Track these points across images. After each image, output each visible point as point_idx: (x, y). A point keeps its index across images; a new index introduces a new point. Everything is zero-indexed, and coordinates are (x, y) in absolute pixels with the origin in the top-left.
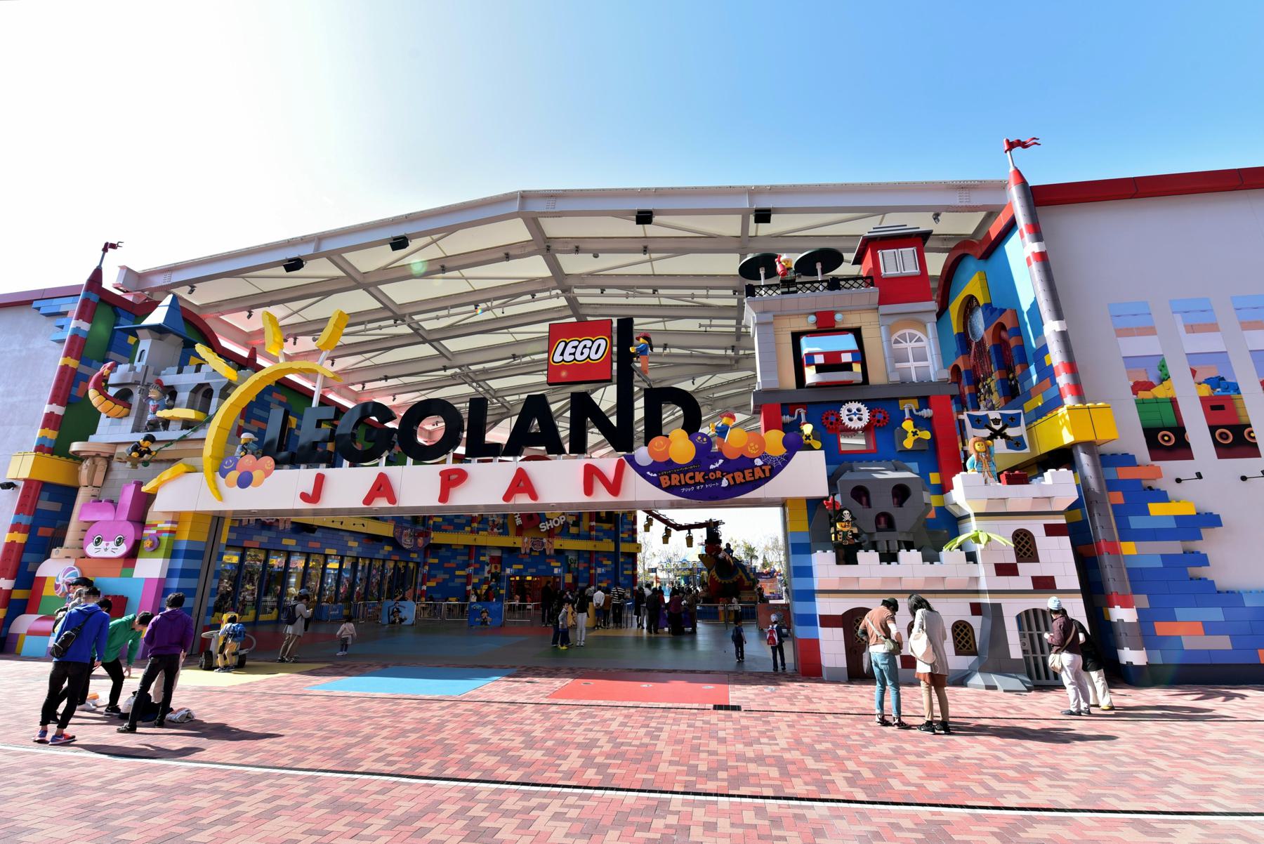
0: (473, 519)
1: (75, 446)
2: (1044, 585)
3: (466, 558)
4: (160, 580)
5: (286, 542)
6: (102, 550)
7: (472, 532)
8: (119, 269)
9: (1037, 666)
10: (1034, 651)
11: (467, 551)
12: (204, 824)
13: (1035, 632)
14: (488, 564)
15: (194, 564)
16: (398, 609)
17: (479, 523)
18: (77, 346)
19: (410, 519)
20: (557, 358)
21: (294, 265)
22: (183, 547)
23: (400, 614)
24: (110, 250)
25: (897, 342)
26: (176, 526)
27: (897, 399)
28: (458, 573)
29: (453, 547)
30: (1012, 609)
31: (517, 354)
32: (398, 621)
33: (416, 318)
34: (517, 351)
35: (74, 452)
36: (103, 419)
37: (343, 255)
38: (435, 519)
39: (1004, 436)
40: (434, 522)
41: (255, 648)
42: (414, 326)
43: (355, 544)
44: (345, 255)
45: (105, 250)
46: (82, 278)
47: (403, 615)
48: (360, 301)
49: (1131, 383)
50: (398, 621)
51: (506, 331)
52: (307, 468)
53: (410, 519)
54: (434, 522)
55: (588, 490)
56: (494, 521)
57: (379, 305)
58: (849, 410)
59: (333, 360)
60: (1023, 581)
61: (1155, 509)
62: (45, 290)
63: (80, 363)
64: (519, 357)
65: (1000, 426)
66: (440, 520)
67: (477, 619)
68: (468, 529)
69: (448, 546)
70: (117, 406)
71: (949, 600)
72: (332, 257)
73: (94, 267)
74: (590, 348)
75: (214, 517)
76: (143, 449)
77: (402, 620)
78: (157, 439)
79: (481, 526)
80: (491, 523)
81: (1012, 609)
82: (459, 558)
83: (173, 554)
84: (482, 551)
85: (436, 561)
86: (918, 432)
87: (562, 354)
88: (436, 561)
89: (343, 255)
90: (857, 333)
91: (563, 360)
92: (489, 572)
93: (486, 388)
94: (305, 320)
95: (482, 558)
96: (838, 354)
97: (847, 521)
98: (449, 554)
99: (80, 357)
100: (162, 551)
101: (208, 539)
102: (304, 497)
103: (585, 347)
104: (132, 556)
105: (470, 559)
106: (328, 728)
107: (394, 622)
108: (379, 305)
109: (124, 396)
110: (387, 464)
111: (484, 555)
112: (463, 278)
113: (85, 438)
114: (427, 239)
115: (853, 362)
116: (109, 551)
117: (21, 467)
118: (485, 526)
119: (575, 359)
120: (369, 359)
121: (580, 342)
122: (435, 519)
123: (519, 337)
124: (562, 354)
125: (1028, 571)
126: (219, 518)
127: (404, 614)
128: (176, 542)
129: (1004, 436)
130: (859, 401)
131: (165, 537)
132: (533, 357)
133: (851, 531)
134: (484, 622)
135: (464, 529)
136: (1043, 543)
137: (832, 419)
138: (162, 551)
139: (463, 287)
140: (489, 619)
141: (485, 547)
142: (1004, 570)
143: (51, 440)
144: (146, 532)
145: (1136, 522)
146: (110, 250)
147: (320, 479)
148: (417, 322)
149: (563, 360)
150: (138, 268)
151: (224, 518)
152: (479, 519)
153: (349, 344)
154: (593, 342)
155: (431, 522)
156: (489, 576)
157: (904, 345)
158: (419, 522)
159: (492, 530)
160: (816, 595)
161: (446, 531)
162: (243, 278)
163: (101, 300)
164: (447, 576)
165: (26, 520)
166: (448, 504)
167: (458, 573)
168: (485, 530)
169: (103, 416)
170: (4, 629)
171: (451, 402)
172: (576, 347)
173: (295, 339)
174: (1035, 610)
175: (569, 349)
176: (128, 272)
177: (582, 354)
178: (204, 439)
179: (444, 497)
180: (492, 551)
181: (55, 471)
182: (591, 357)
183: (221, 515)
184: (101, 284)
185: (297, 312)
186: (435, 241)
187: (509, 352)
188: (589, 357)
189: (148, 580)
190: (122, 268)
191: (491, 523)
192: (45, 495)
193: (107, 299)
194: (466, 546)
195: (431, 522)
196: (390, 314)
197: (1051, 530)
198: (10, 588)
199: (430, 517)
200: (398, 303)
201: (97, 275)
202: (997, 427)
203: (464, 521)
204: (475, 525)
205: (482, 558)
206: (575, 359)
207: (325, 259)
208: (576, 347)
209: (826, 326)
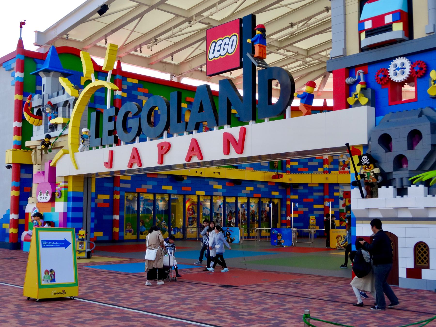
1: (49, 143)
3: (321, 194)
5: (164, 188)
6: (42, 198)
7: (324, 172)
8: (35, 32)
11: (322, 188)
14: (342, 199)
16: (229, 232)
17: (332, 164)
20: (211, 56)
23: (231, 236)
26: (66, 184)
28: (315, 206)
31: (294, 22)
33: (205, 14)
34: (294, 19)
36: (35, 128)
40: (291, 166)
41: (95, 249)
42: (207, 21)
43: (220, 187)
45: (21, 27)
46: (14, 48)
47: (232, 237)
51: (277, 5)
54: (291, 166)
55: (227, 152)
56: (344, 161)
57: (173, 16)
59: (172, 56)
63: (23, 96)
64: (296, 24)
66: (296, 163)
67: (275, 241)
68: (320, 169)
69: (305, 185)
70: (36, 119)
71: (415, 225)
74: (228, 44)
75: (85, 178)
76: (47, 143)
77: (232, 240)
78: (52, 136)
79: (332, 166)
80: (341, 164)
83: (68, 199)
84: (335, 188)
85: (296, 197)
86: (356, 94)
87: (213, 53)
88: (296, 197)
92: (344, 205)
93: (296, 50)
94: (142, 34)
95: (336, 194)
97: (365, 164)
98: (307, 191)
100: (63, 198)
101: (84, 190)
103: (225, 44)
104: (53, 200)
105: (324, 195)
108: (173, 16)
109: (39, 115)
110: (168, 137)
111: (338, 191)
115: (394, 22)
116: (45, 198)
117: (9, 159)
118: (336, 166)
119: (220, 55)
120: (197, 48)
121: (223, 40)
122: (292, 163)
124: (213, 53)
126: (88, 178)
131: (63, 190)
132: (317, 17)
133: (373, 172)
134: (279, 243)
135: (317, 170)
137: (417, 68)
138: (63, 198)
140: (283, 241)
141: (337, 185)
143: (19, 141)
150: (42, 30)
151: (91, 178)
152: (330, 161)
154: (230, 39)
156: (345, 208)
159: (343, 169)
160: (356, 221)
161: (301, 172)
162: (93, 19)
163: (25, 57)
164: (307, 209)
165: (17, 184)
166: (191, 162)
167: (315, 206)
169: (34, 126)
170: (19, 239)
171: (279, 65)
172: (220, 45)
173: (141, 48)
175: (217, 48)
176: (39, 34)
177: (224, 49)
179: (161, 160)
180: (344, 187)
183: (89, 176)
184: (24, 48)
188: (227, 51)
189: (60, 213)
190: (36, 32)
191: (341, 164)
192: (23, 170)
193: (29, 55)
194: (320, 184)
195: (288, 166)
196: (183, 19)
198: (17, 219)
199: (288, 162)
201: (20, 43)
203: (316, 163)
204: (326, 166)
205: (336, 194)
206: (220, 55)
208: (220, 45)
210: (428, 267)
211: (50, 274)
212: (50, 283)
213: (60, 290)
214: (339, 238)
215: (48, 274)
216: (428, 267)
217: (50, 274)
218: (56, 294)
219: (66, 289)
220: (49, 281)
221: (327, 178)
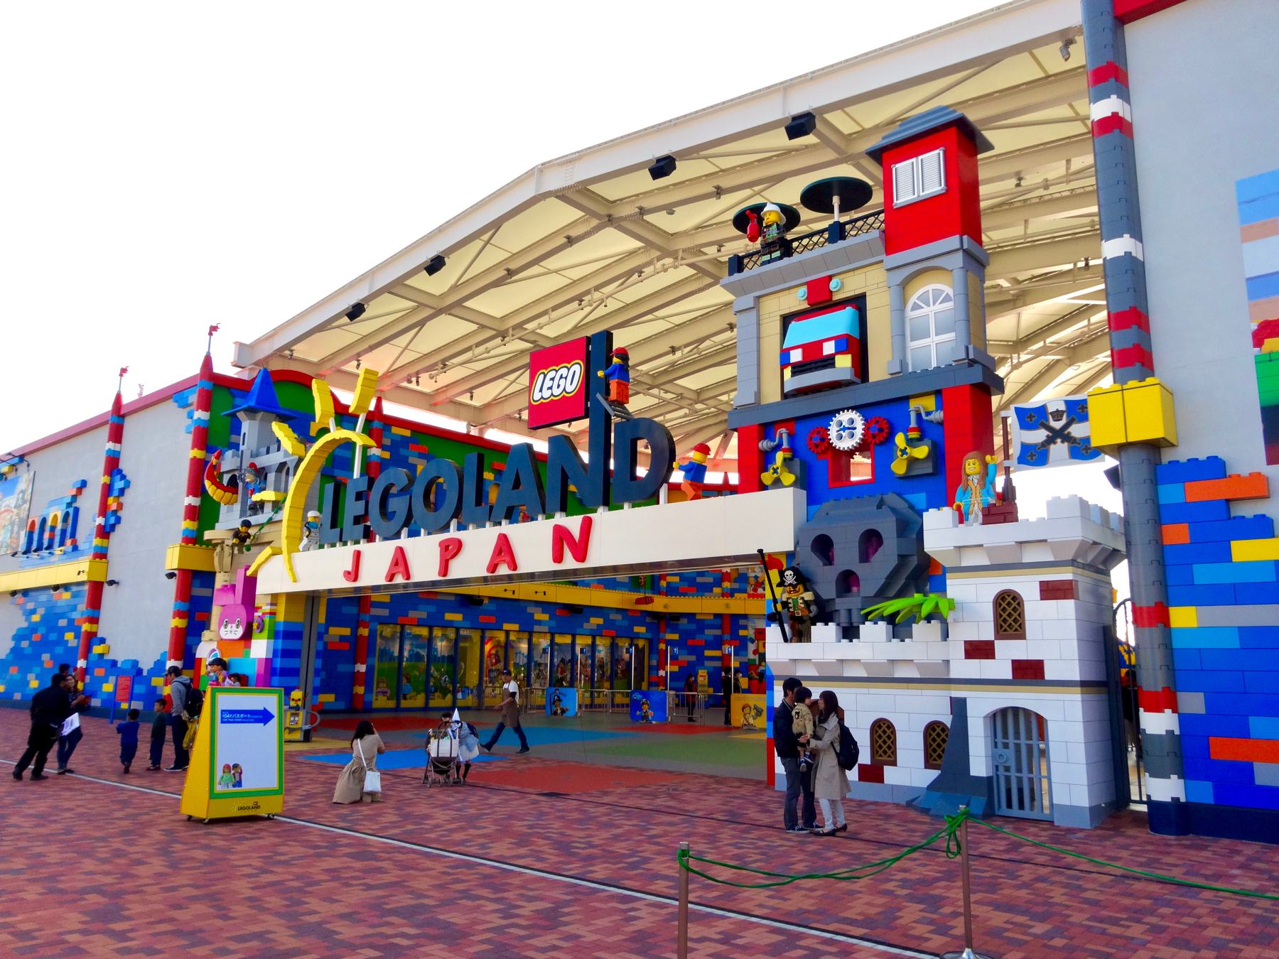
0: (725, 577)
2: (1028, 672)
4: (267, 659)
5: (449, 616)
7: (723, 595)
9: (1020, 791)
10: (1019, 770)
11: (718, 622)
12: (473, 941)
13: (1023, 741)
14: (753, 642)
15: (293, 645)
18: (203, 438)
19: (627, 581)
20: (537, 396)
21: (355, 312)
22: (281, 628)
24: (213, 332)
25: (916, 307)
26: (274, 607)
27: (906, 399)
28: (708, 653)
29: (698, 617)
30: (981, 705)
32: (559, 711)
33: (530, 326)
34: (677, 340)
35: (207, 540)
36: (223, 508)
37: (406, 282)
38: (670, 579)
39: (1067, 438)
40: (668, 584)
42: (533, 338)
43: (545, 617)
44: (408, 282)
45: (210, 334)
48: (445, 330)
49: (1254, 326)
50: (559, 711)
51: (650, 317)
52: (633, 507)
53: (627, 581)
54: (668, 584)
55: (558, 558)
58: (840, 423)
59: (471, 393)
60: (1000, 667)
61: (1245, 551)
62: (92, 420)
64: (679, 349)
65: (1064, 421)
66: (677, 579)
69: (691, 616)
72: (392, 291)
73: (204, 354)
74: (566, 378)
77: (563, 711)
78: (253, 523)
79: (736, 586)
80: (752, 581)
81: (981, 705)
82: (708, 632)
83: (275, 635)
84: (742, 622)
85: (676, 637)
87: (541, 391)
88: (676, 637)
89: (406, 282)
90: (858, 302)
91: (542, 397)
95: (742, 633)
96: (818, 345)
97: (790, 585)
98: (693, 626)
99: (209, 449)
100: (266, 633)
102: (347, 574)
103: (561, 377)
104: (247, 637)
106: (642, 854)
107: (555, 713)
109: (233, 486)
111: (745, 628)
112: (550, 272)
113: (213, 528)
114: (478, 244)
117: (172, 560)
118: (743, 585)
119: (552, 395)
121: (557, 371)
122: (670, 579)
123: (678, 320)
124: (541, 391)
125: (1008, 651)
126: (313, 597)
127: (565, 703)
128: (276, 623)
129: (1067, 438)
130: (853, 408)
133: (802, 598)
135: (712, 591)
136: (1036, 610)
137: (874, 429)
138: (266, 633)
139: (556, 282)
141: (745, 616)
142: (979, 650)
144: (256, 614)
145: (1204, 574)
146: (213, 332)
147: (358, 555)
148: (533, 332)
149: (542, 397)
150: (248, 341)
152: (734, 576)
153: (482, 370)
154: (569, 369)
155: (663, 584)
157: (925, 310)
158: (425, 595)
159: (755, 590)
160: (775, 682)
164: (693, 658)
165: (184, 606)
167: (708, 653)
168: (744, 591)
169: (222, 504)
172: (553, 379)
173: (418, 378)
174: (1016, 710)
175: (548, 383)
177: (559, 386)
178: (281, 521)
179: (444, 570)
181: (197, 562)
182: (567, 390)
185: (406, 348)
186: (488, 242)
187: (664, 346)
188: (564, 389)
189: (260, 660)
191: (752, 581)
194: (716, 616)
195: (663, 584)
196: (491, 333)
197: (1050, 591)
200: (499, 316)
201: (208, 362)
202: (1057, 425)
203: (711, 580)
204: (726, 585)
205: (742, 633)
206: (552, 395)
207: (386, 295)
208: (553, 379)
209: (821, 301)
210: (894, 763)
211: (232, 772)
212: (231, 789)
213: (249, 802)
214: (747, 710)
215: (230, 772)
216: (894, 763)
217: (232, 772)
218: (241, 809)
219: (262, 801)
220: (230, 785)
221: (727, 606)
